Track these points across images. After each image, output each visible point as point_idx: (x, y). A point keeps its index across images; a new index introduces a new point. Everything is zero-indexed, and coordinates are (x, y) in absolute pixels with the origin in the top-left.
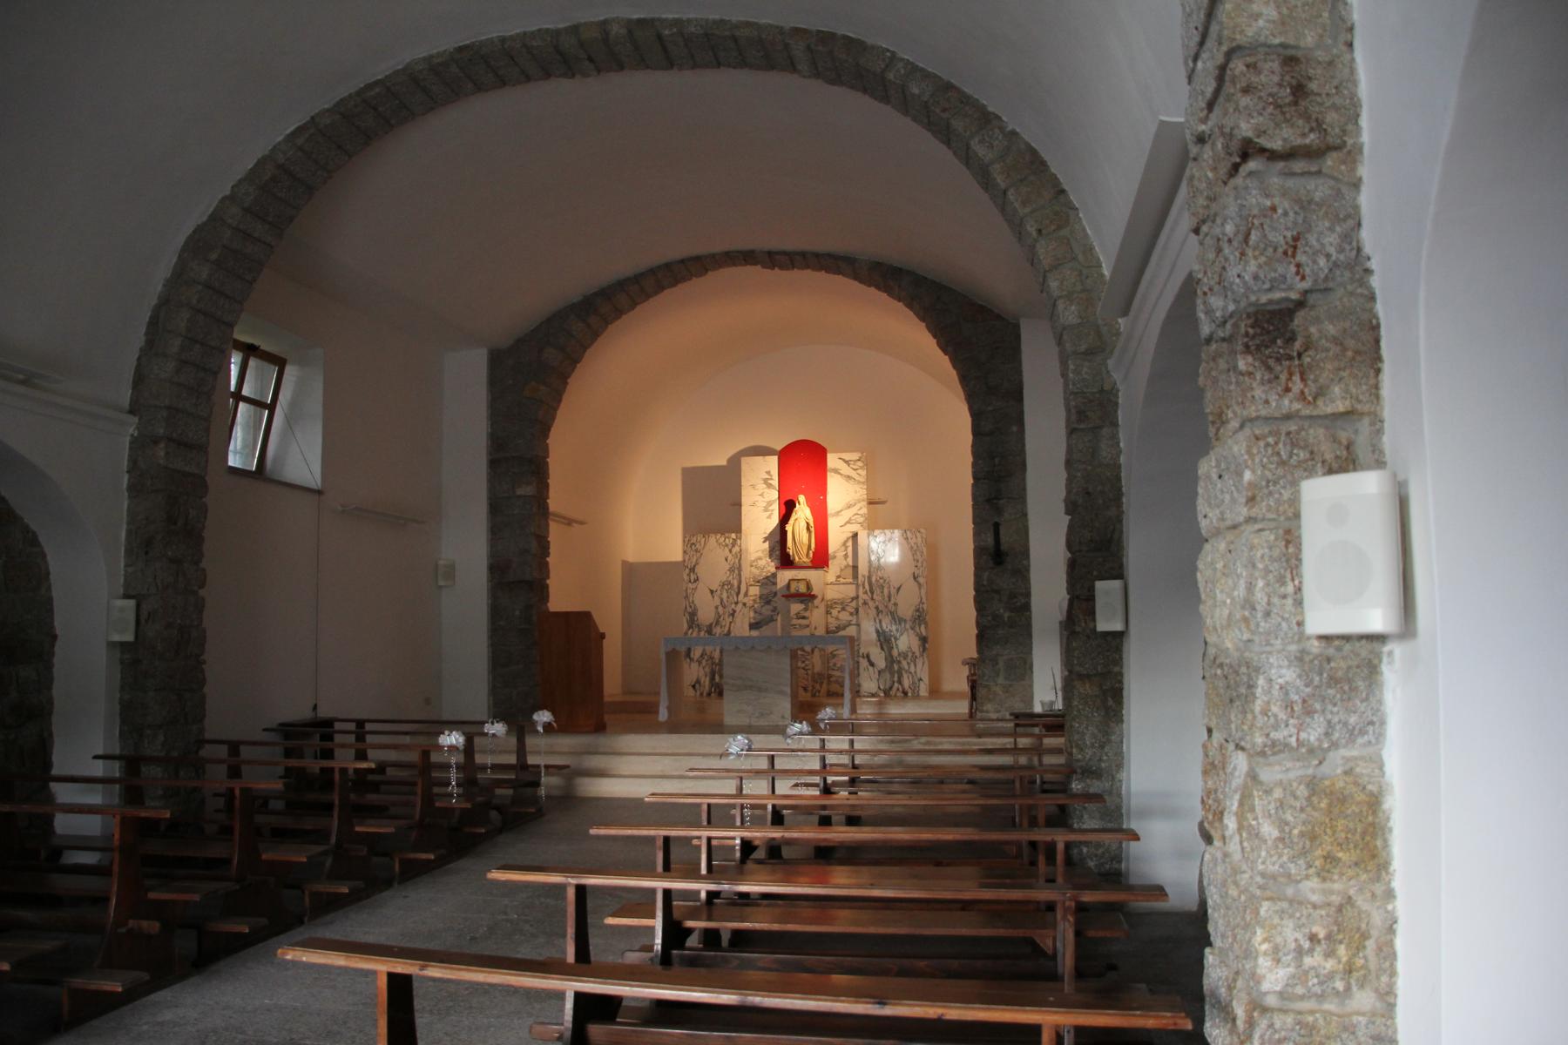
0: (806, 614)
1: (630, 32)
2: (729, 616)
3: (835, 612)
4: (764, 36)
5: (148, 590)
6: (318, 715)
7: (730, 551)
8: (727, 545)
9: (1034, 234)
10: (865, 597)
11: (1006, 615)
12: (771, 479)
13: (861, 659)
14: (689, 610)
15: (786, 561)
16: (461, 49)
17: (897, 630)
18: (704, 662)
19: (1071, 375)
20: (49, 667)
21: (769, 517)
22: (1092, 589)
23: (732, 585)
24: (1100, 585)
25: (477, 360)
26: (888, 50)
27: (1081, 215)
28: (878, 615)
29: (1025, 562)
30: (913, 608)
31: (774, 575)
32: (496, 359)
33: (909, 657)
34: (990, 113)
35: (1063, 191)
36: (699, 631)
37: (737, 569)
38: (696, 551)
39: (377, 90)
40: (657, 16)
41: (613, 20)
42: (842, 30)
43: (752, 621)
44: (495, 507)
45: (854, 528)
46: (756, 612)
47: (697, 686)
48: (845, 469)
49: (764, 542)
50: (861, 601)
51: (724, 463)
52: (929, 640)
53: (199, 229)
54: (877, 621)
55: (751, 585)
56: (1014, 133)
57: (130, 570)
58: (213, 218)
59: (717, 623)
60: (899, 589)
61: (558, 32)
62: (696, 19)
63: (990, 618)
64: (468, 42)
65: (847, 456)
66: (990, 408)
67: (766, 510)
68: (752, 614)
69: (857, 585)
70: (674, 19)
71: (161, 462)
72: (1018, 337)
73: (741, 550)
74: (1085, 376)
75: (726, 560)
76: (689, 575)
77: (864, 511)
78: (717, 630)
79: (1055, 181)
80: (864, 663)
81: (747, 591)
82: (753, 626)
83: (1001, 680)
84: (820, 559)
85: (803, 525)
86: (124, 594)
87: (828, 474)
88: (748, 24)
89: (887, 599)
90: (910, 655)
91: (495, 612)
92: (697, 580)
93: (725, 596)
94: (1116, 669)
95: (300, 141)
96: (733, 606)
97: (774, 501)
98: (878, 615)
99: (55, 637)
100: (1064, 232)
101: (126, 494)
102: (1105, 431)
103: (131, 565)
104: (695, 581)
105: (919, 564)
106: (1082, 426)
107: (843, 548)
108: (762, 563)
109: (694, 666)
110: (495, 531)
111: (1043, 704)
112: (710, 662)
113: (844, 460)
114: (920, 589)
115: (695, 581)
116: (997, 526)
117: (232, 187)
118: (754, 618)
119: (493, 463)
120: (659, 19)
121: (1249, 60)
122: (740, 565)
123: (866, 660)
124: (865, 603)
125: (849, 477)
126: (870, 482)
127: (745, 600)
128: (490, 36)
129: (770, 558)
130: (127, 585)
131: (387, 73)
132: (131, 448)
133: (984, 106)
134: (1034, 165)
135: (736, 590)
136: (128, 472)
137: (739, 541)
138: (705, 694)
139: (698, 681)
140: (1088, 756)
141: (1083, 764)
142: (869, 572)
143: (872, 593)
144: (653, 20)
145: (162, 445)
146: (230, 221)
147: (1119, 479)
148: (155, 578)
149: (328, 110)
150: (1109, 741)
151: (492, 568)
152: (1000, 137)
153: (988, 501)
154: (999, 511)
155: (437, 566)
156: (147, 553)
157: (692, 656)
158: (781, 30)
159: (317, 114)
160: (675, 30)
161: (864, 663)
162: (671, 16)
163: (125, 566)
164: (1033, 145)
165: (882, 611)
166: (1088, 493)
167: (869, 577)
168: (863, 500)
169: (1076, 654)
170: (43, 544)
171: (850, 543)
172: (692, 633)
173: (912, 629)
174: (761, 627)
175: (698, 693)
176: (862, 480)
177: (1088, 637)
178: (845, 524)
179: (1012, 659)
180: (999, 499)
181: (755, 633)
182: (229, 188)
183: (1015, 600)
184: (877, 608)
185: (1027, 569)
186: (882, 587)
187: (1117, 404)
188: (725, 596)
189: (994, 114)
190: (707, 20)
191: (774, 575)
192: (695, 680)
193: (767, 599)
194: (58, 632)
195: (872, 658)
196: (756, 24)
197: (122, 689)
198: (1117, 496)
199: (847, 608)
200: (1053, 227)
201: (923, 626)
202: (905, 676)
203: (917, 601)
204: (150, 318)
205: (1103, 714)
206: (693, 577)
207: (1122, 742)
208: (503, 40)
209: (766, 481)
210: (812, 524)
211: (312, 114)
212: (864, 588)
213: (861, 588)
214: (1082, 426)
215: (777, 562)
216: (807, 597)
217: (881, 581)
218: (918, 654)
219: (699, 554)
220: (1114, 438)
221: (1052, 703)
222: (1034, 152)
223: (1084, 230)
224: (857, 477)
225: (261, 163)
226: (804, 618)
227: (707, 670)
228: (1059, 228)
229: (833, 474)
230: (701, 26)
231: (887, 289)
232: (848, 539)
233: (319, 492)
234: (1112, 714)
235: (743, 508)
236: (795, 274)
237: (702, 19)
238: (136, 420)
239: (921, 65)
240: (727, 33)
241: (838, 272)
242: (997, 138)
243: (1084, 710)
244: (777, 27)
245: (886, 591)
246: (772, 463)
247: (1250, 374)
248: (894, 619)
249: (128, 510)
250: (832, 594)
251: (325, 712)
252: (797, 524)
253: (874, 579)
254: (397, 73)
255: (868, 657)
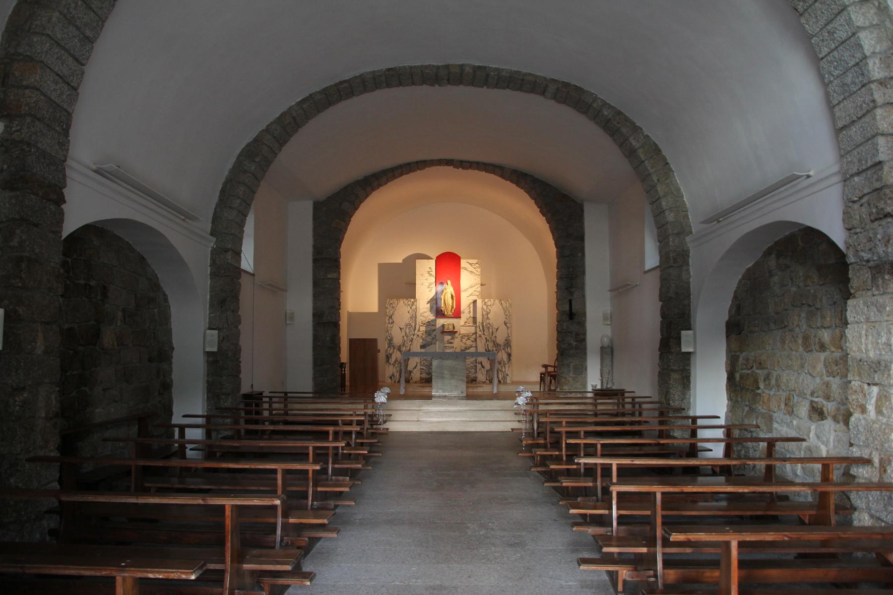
0: (452, 341)
1: (474, 71)
2: (410, 342)
3: (464, 340)
4: (538, 81)
5: (223, 325)
6: (254, 390)
7: (411, 308)
8: (409, 305)
9: (656, 181)
10: (480, 333)
11: (574, 343)
12: (432, 271)
13: (478, 365)
14: (389, 338)
15: (439, 313)
16: (389, 70)
17: (496, 350)
18: (396, 365)
19: (671, 243)
20: (171, 363)
21: (430, 291)
22: (680, 334)
23: (412, 326)
24: (683, 333)
25: (307, 208)
26: (594, 94)
27: (675, 174)
28: (486, 342)
29: (583, 319)
30: (504, 339)
31: (435, 321)
32: (318, 207)
33: (502, 363)
34: (637, 126)
35: (668, 163)
36: (394, 349)
37: (414, 317)
38: (393, 307)
39: (345, 85)
40: (487, 65)
41: (466, 65)
42: (573, 82)
43: (421, 344)
44: (316, 284)
45: (475, 298)
46: (423, 340)
47: (392, 377)
48: (470, 268)
49: (427, 304)
50: (478, 335)
51: (401, 261)
52: (512, 355)
53: (248, 145)
54: (486, 345)
55: (421, 326)
56: (647, 136)
57: (212, 315)
58: (256, 140)
59: (404, 345)
60: (497, 329)
61: (438, 67)
62: (506, 69)
63: (567, 345)
64: (393, 67)
65: (471, 261)
66: (568, 244)
67: (429, 287)
68: (421, 341)
69: (476, 327)
70: (496, 68)
71: (229, 261)
72: (583, 211)
73: (416, 308)
74: (677, 244)
75: (409, 312)
76: (389, 320)
77: (479, 289)
78: (403, 349)
79: (664, 158)
80: (479, 366)
81: (419, 329)
82: (422, 347)
83: (571, 375)
84: (457, 314)
85: (450, 296)
86: (209, 328)
87: (461, 270)
88: (530, 74)
89: (491, 334)
90: (502, 362)
91: (316, 338)
92: (393, 322)
93: (408, 331)
94: (688, 368)
95: (305, 106)
96: (412, 336)
97: (433, 283)
98: (486, 342)
99: (173, 348)
100: (668, 181)
101: (209, 277)
102: (684, 267)
103: (212, 313)
104: (392, 323)
105: (508, 317)
106: (675, 265)
107: (468, 308)
108: (426, 314)
109: (391, 367)
110: (316, 296)
111: (592, 386)
112: (399, 365)
113: (469, 263)
114: (508, 329)
115: (392, 323)
116: (570, 301)
117: (267, 126)
118: (422, 343)
119: (315, 261)
120: (488, 67)
121: (891, 190)
122: (416, 315)
123: (480, 365)
124: (480, 336)
125: (471, 272)
126: (482, 275)
127: (418, 333)
128: (404, 65)
129: (430, 312)
130: (210, 323)
131: (351, 77)
132: (211, 254)
133: (635, 123)
134: (655, 151)
135: (414, 328)
136: (210, 266)
137: (415, 303)
138: (396, 382)
139: (393, 375)
140: (676, 404)
141: (674, 407)
142: (483, 320)
143: (484, 331)
144: (485, 68)
145: (230, 253)
146: (267, 142)
147: (689, 288)
148: (227, 320)
149: (319, 92)
150: (685, 398)
151: (314, 315)
152: (642, 137)
153: (567, 289)
154: (571, 293)
155: (286, 313)
156: (221, 307)
157: (390, 362)
158: (545, 79)
159: (313, 93)
160: (496, 73)
161: (479, 366)
162: (494, 66)
163: (209, 314)
164: (656, 142)
165: (488, 340)
166: (677, 293)
167: (482, 323)
168: (479, 284)
169: (672, 361)
170: (170, 302)
171: (472, 306)
172: (390, 350)
173: (504, 349)
174: (426, 347)
175: (393, 381)
176: (479, 274)
177: (677, 354)
178: (470, 296)
179: (576, 365)
180: (572, 288)
181: (423, 350)
182: (265, 126)
183: (579, 337)
184: (486, 339)
185: (585, 321)
186: (489, 328)
187: (689, 256)
188: (408, 331)
189: (639, 127)
190: (511, 70)
191: (435, 321)
192: (391, 374)
193: (428, 333)
194: (175, 346)
195: (483, 364)
196: (534, 74)
197: (208, 375)
198: (688, 296)
199: (471, 338)
200: (664, 179)
201: (509, 348)
202: (500, 373)
203: (506, 335)
204: (222, 188)
205: (682, 386)
206: (391, 321)
207: (690, 398)
208: (411, 67)
209: (429, 272)
210: (454, 295)
211: (311, 93)
212: (480, 328)
213: (478, 328)
214: (675, 265)
215: (434, 314)
216: (453, 333)
217: (489, 325)
218: (506, 362)
219: (394, 309)
220: (688, 270)
221: (596, 386)
222: (656, 145)
223: (676, 180)
224: (475, 272)
225: (283, 115)
226: (451, 343)
227: (398, 369)
228: (666, 179)
229: (463, 270)
230: (508, 73)
231: (518, 184)
232: (471, 303)
233: (253, 275)
234: (686, 386)
235: (417, 286)
236: (470, 172)
237: (509, 69)
238: (214, 239)
239: (608, 102)
240: (520, 77)
241: (493, 172)
242: (641, 138)
243: (675, 385)
244: (544, 77)
245: (491, 330)
246: (432, 264)
247: (889, 280)
248: (494, 344)
249: (210, 285)
250: (463, 331)
251: (257, 389)
252: (447, 294)
253: (485, 324)
254: (355, 77)
255: (481, 363)
